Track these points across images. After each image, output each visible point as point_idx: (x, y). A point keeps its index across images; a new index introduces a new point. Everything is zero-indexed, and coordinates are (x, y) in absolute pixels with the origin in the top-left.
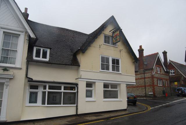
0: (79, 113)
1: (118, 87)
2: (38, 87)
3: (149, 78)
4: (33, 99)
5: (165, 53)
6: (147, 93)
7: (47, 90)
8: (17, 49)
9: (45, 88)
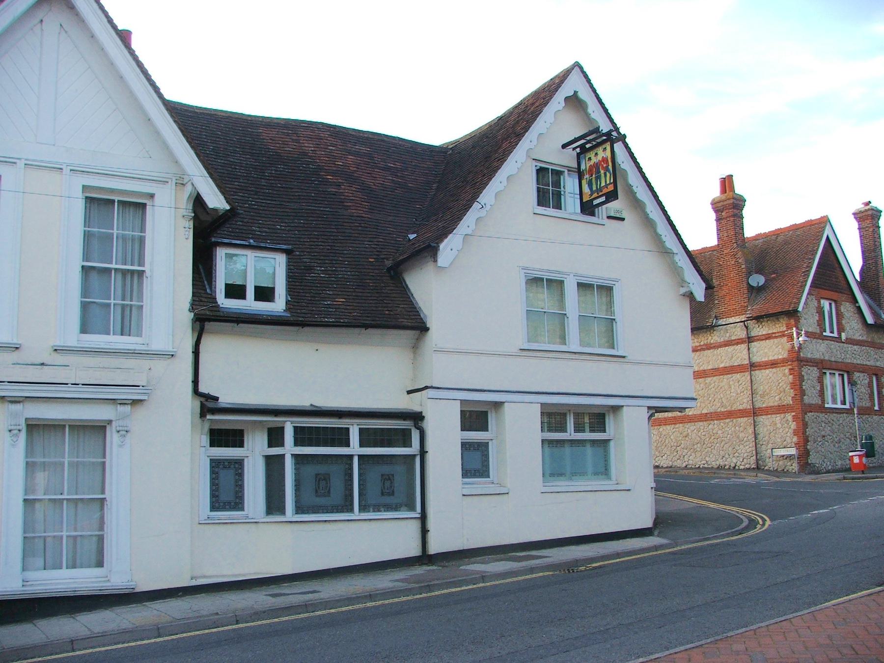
0: (434, 548)
1: (610, 422)
2: (604, 419)
3: (773, 364)
4: (225, 492)
5: (868, 218)
6: (766, 452)
7: (289, 448)
8: (141, 263)
9: (275, 437)
